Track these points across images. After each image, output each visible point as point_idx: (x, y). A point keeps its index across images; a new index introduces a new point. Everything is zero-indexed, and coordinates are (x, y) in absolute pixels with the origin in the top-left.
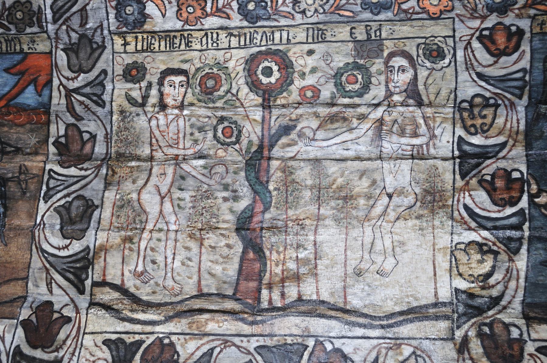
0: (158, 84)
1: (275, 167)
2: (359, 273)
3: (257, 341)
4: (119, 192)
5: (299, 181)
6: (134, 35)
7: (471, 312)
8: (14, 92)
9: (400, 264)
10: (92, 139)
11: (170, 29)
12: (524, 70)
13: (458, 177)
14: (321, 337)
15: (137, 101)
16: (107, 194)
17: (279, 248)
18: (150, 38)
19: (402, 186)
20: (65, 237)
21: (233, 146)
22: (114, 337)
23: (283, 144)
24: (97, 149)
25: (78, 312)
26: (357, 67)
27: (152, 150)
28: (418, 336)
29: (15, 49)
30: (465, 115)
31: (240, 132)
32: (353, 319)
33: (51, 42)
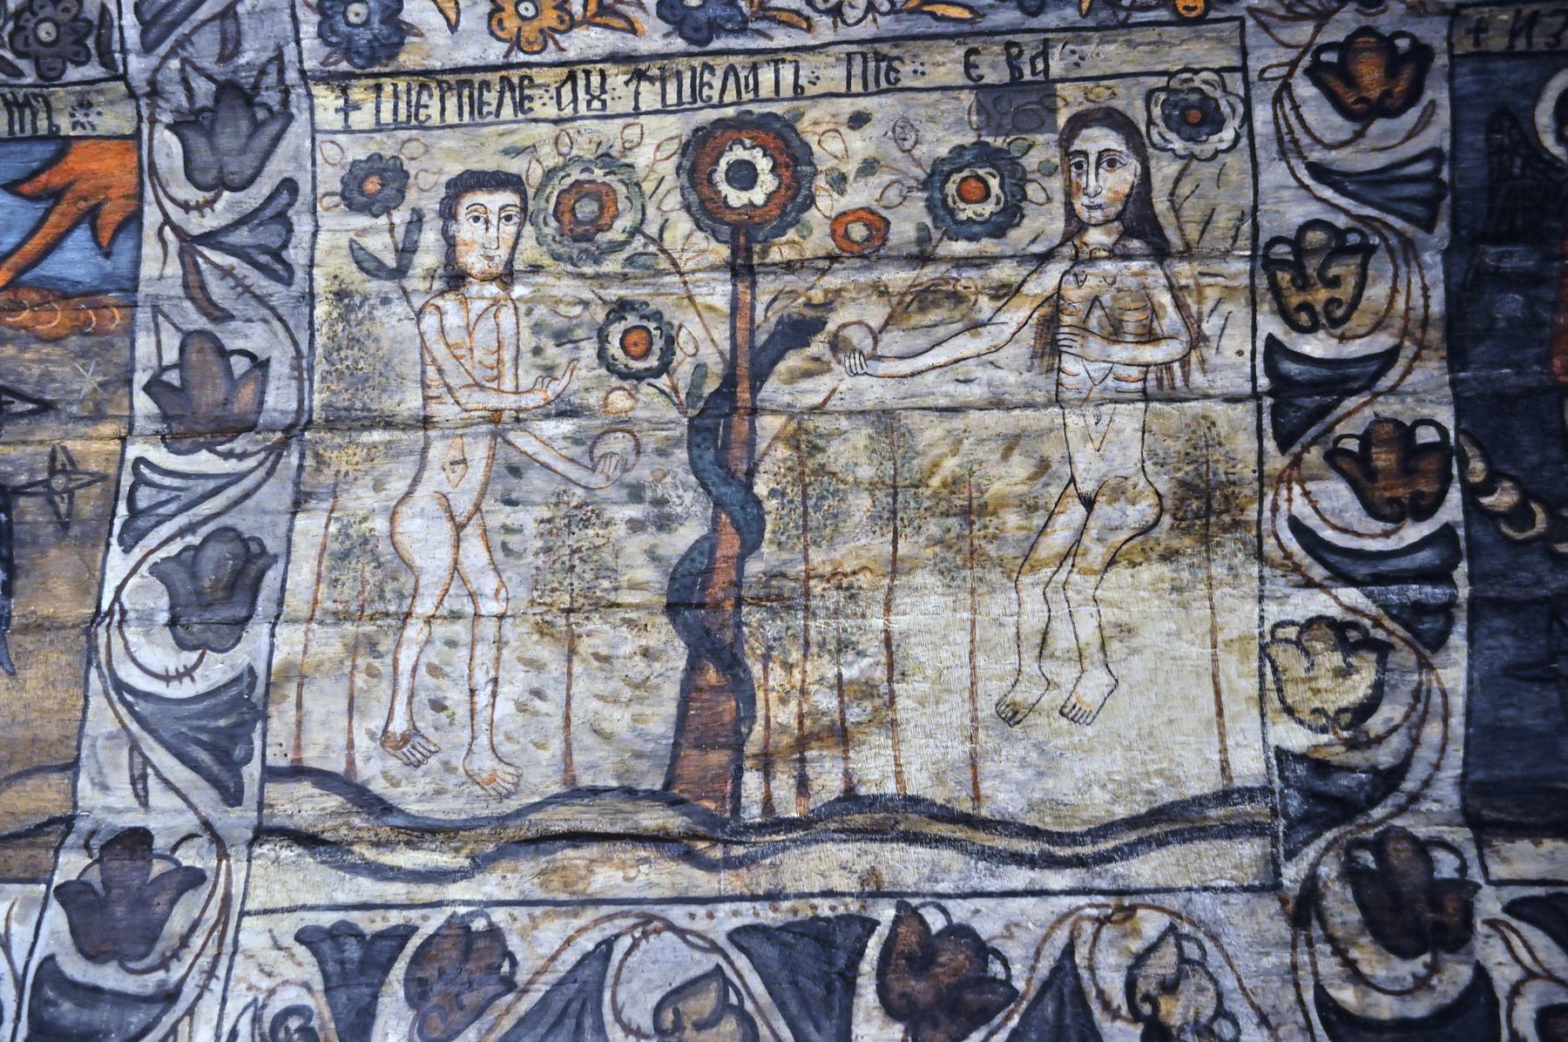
0: (441, 214)
1: (771, 433)
2: (1011, 715)
3: (736, 913)
4: (334, 515)
6: (371, 82)
7: (1324, 814)
9: (1123, 686)
11: (471, 63)
12: (1434, 154)
13: (1270, 445)
14: (915, 895)
16: (301, 521)
17: (786, 652)
19: (1122, 473)
20: (182, 645)
21: (652, 381)
22: (328, 919)
23: (791, 371)
24: (270, 400)
27: (426, 399)
30: (1284, 277)
31: (671, 341)
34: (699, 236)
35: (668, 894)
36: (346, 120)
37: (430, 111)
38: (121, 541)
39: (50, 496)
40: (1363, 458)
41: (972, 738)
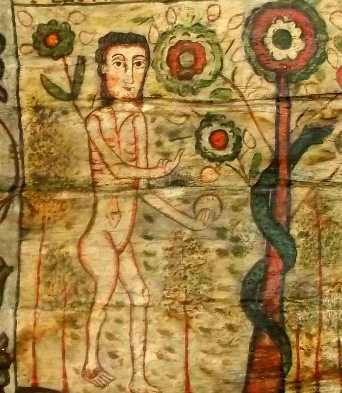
1: (301, 198)
4: (45, 243)
5: (339, 221)
15: (61, 91)
16: (25, 247)
17: (309, 328)
21: (228, 162)
23: (311, 158)
27: (93, 171)
31: (239, 139)
34: (256, 78)
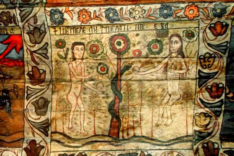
0: (72, 49)
2: (157, 125)
3: (119, 152)
4: (58, 95)
6: (59, 27)
7: (200, 139)
8: (6, 52)
9: (173, 122)
10: (44, 73)
11: (75, 25)
12: (227, 42)
13: (197, 87)
14: (143, 150)
15: (62, 57)
16: (53, 96)
17: (126, 117)
18: (66, 28)
20: (38, 115)
22: (62, 153)
24: (46, 77)
25: (47, 144)
26: (158, 41)
27: (71, 77)
28: (180, 148)
29: (4, 33)
30: (202, 61)
31: (108, 69)
32: (155, 143)
33: (21, 30)
34: (112, 54)
35: (110, 149)
36: (55, 33)
37: (69, 32)
38: (26, 99)
39: (14, 92)
40: (211, 89)
41: (152, 128)
